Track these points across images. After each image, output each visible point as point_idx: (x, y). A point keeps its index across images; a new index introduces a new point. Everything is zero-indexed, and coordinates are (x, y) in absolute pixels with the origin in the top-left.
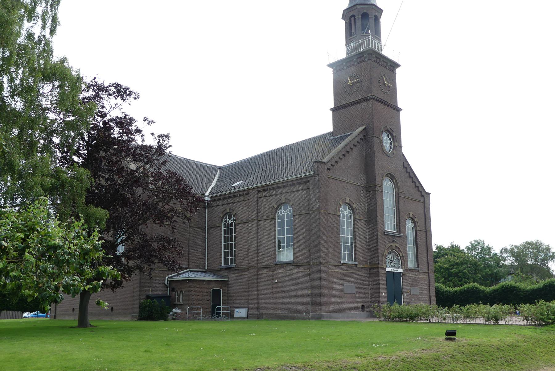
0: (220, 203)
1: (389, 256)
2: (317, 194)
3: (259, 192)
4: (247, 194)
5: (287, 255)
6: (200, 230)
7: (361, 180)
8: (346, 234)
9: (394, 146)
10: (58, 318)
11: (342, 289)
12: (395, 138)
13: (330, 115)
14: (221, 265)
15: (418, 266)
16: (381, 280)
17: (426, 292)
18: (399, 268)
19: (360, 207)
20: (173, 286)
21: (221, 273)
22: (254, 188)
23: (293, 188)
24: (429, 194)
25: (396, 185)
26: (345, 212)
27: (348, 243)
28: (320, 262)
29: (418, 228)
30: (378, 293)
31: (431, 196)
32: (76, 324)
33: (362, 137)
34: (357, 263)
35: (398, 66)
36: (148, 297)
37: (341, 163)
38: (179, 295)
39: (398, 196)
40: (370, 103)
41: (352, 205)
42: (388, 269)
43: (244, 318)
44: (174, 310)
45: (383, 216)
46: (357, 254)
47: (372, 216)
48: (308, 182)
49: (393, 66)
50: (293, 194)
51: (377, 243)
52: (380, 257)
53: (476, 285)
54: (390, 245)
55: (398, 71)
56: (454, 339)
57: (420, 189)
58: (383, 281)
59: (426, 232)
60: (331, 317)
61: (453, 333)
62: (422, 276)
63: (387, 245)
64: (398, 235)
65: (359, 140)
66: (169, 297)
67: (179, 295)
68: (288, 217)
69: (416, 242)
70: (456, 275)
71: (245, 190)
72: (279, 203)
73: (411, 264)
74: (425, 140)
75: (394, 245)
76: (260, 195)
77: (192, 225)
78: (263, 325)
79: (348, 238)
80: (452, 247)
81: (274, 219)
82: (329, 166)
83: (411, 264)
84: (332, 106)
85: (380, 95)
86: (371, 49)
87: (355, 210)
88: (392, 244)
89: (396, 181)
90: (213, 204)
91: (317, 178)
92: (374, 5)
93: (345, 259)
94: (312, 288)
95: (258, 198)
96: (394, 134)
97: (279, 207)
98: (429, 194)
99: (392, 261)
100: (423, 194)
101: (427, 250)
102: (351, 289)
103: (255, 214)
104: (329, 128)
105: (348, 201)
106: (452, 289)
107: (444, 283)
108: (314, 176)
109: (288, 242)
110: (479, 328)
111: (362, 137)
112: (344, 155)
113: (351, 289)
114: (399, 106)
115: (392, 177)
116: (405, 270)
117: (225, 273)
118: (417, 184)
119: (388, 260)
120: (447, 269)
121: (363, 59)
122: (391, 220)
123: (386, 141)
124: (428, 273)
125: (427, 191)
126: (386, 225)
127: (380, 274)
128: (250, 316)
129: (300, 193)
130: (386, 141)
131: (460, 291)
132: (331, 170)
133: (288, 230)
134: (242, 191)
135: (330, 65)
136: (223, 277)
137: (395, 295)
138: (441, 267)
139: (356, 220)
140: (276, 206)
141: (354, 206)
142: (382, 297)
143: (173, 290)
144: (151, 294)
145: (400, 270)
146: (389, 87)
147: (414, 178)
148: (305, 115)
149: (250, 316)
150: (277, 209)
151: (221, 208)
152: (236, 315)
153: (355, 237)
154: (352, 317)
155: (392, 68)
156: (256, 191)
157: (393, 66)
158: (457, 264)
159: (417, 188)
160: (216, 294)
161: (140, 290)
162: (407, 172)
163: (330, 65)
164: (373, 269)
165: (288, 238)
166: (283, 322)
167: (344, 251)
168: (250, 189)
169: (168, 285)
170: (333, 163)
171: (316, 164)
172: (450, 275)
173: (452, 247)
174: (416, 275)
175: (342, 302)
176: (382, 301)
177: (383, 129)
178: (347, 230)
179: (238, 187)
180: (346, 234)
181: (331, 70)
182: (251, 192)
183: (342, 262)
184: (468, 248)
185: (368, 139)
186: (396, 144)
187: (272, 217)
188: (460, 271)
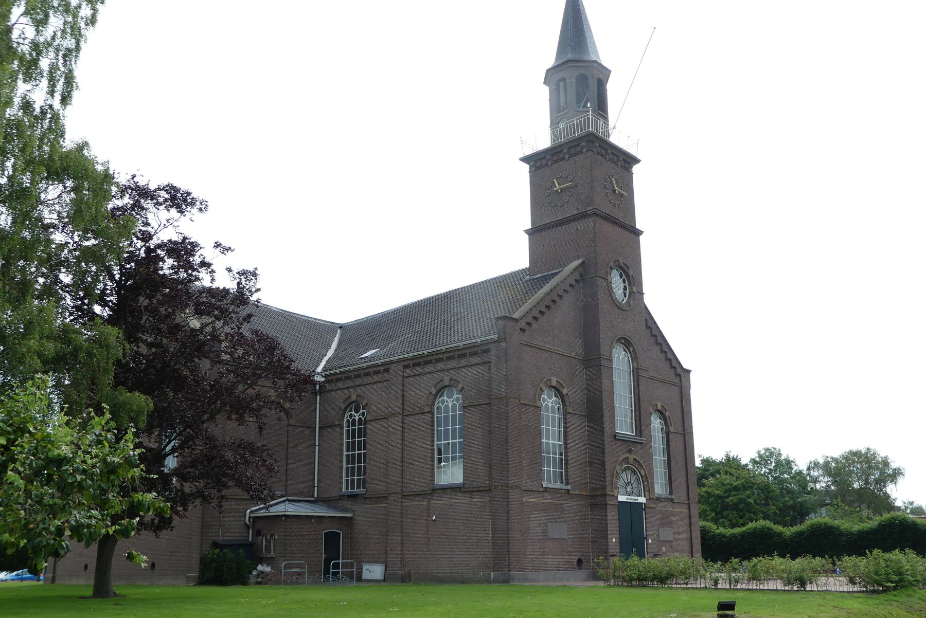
0: (340, 385)
1: (624, 475)
2: (503, 372)
4: (387, 370)
5: (452, 474)
6: (306, 431)
9: (631, 293)
10: (58, 582)
11: (545, 532)
14: (341, 490)
15: (671, 493)
16: (609, 516)
17: (685, 536)
18: (640, 495)
21: (340, 503)
22: (399, 361)
24: (688, 372)
25: (634, 357)
28: (507, 486)
29: (672, 429)
30: (605, 537)
32: (89, 592)
33: (578, 277)
34: (569, 487)
35: (636, 161)
36: (215, 545)
37: (542, 320)
41: (664, 411)
42: (622, 498)
44: (260, 567)
45: (612, 408)
50: (463, 371)
51: (603, 453)
55: (636, 169)
58: (612, 516)
60: (526, 580)
61: (731, 606)
62: (678, 509)
65: (573, 283)
66: (252, 545)
68: (454, 410)
69: (668, 451)
70: (735, 507)
71: (383, 364)
72: (440, 386)
73: (660, 489)
75: (631, 457)
76: (408, 372)
77: (292, 422)
81: (432, 412)
82: (523, 324)
83: (660, 489)
84: (529, 226)
85: (606, 209)
86: (592, 134)
87: (566, 398)
89: (634, 350)
91: (503, 344)
93: (549, 481)
95: (404, 377)
96: (631, 273)
97: (440, 392)
98: (688, 372)
99: (628, 483)
100: (679, 371)
102: (561, 531)
103: (399, 404)
105: (554, 384)
106: (729, 532)
107: (715, 521)
109: (454, 452)
110: (773, 596)
111: (578, 277)
112: (548, 307)
114: (639, 225)
115: (627, 344)
116: (650, 499)
117: (348, 504)
119: (621, 483)
120: (720, 497)
121: (578, 149)
122: (626, 416)
123: (617, 284)
124: (689, 504)
125: (685, 367)
126: (618, 424)
127: (608, 507)
128: (388, 578)
130: (617, 284)
131: (742, 535)
132: (527, 332)
133: (454, 430)
134: (377, 365)
135: (525, 159)
137: (633, 542)
138: (709, 494)
140: (434, 391)
141: (565, 391)
142: (612, 545)
143: (258, 533)
144: (220, 539)
145: (642, 500)
146: (622, 195)
148: (476, 235)
149: (388, 578)
152: (366, 575)
153: (566, 443)
154: (562, 579)
157: (628, 161)
158: (736, 488)
160: (332, 540)
162: (653, 336)
163: (525, 159)
164: (597, 498)
168: (392, 362)
169: (251, 525)
170: (530, 319)
172: (725, 507)
175: (544, 554)
176: (611, 552)
177: (611, 264)
179: (370, 359)
181: (526, 167)
182: (393, 367)
183: (545, 485)
184: (753, 461)
185: (588, 278)
186: (634, 289)
187: (427, 409)
188: (741, 501)
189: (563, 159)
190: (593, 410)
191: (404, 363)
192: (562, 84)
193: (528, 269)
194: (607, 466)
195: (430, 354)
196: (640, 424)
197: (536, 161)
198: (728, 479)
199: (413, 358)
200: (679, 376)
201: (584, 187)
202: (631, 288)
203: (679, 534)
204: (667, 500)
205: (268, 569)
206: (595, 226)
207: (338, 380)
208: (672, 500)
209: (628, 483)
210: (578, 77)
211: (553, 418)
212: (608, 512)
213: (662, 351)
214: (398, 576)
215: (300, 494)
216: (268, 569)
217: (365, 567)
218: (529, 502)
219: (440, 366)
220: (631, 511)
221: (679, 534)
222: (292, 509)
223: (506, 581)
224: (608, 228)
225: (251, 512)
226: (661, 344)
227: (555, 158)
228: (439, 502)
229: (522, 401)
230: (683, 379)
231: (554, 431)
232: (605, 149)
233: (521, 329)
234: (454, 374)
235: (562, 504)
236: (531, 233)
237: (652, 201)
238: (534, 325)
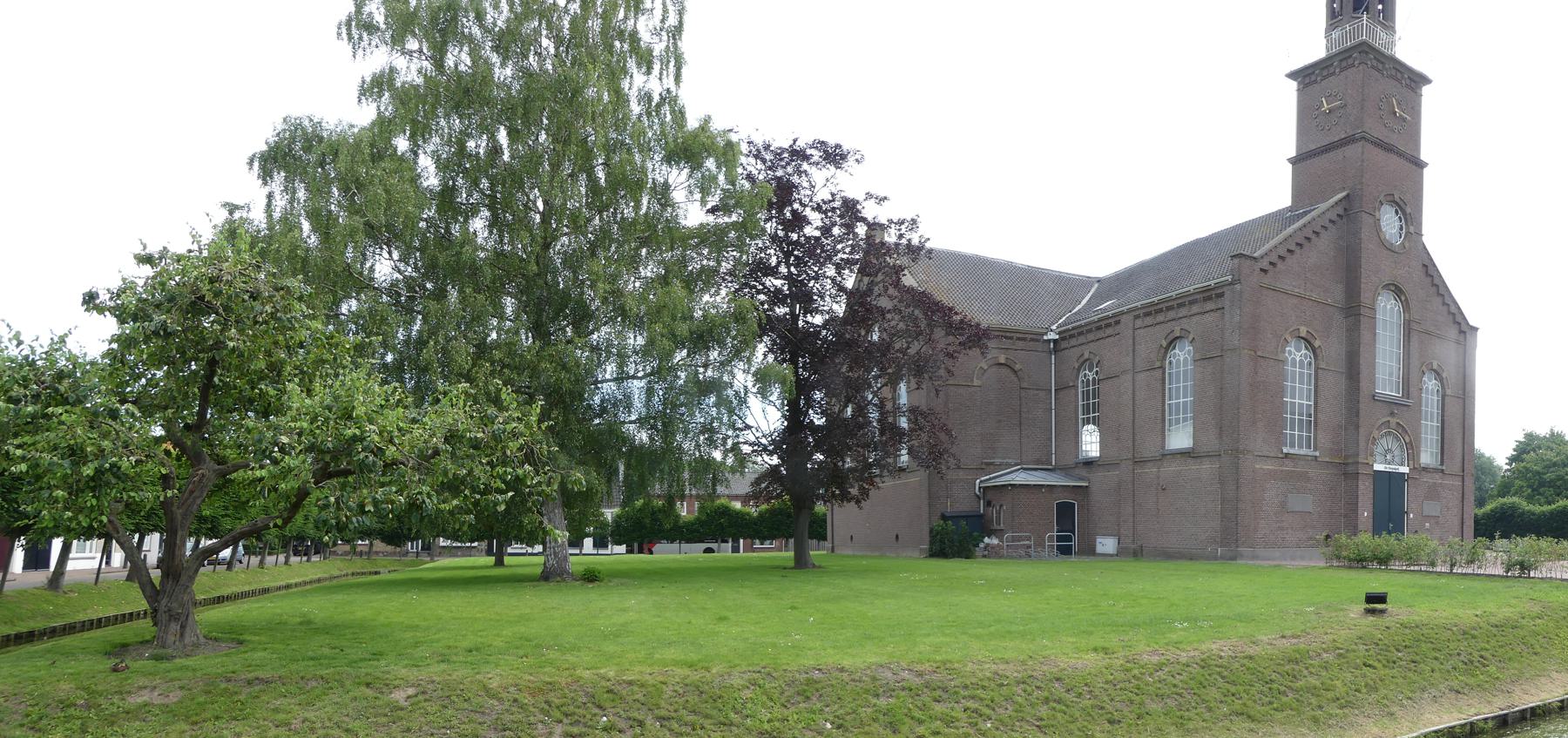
0: (1073, 342)
1: (1383, 441)
2: (1237, 318)
3: (1137, 317)
4: (1118, 323)
5: (1180, 439)
6: (1042, 394)
7: (1337, 294)
8: (1298, 396)
9: (1408, 233)
10: (837, 551)
11: (1283, 504)
12: (1410, 214)
16: (1361, 487)
17: (1456, 511)
19: (1334, 349)
20: (989, 497)
21: (1077, 471)
22: (1130, 311)
23: (1195, 309)
24: (1476, 329)
25: (1406, 307)
26: (1296, 354)
27: (1301, 414)
28: (1237, 450)
29: (1449, 392)
30: (1356, 511)
32: (792, 564)
33: (1341, 212)
35: (1425, 80)
36: (944, 517)
37: (1291, 260)
38: (999, 513)
39: (1408, 329)
42: (1378, 467)
44: (986, 540)
45: (1373, 365)
47: (1354, 369)
48: (1221, 295)
49: (1414, 81)
50: (1195, 319)
52: (1362, 444)
55: (1426, 90)
56: (1382, 611)
57: (1459, 319)
58: (1365, 489)
60: (1254, 557)
61: (1381, 599)
64: (1405, 401)
65: (1334, 218)
66: (981, 516)
67: (999, 513)
68: (1185, 364)
70: (1551, 484)
71: (1114, 316)
72: (1171, 337)
73: (1427, 458)
74: (1465, 220)
75: (1393, 421)
76: (1139, 323)
77: (1025, 385)
78: (1132, 566)
79: (1301, 405)
80: (1552, 434)
81: (1162, 368)
82: (1264, 264)
83: (1427, 458)
84: (1293, 154)
85: (1377, 132)
86: (1364, 43)
90: (1064, 345)
91: (1238, 287)
93: (1292, 446)
94: (1223, 500)
96: (1408, 210)
97: (1172, 343)
98: (1476, 329)
99: (1388, 451)
100: (1464, 328)
102: (1304, 502)
103: (1130, 359)
104: (1281, 198)
105: (1303, 334)
106: (1537, 509)
107: (1530, 499)
108: (1231, 284)
109: (1185, 412)
110: (1490, 585)
111: (1341, 212)
112: (1300, 245)
113: (1304, 502)
114: (1423, 157)
115: (1398, 291)
117: (1083, 472)
118: (1453, 309)
119: (1379, 449)
120: (1538, 473)
121: (1350, 61)
122: (1391, 375)
123: (1389, 222)
126: (1379, 383)
128: (1121, 553)
129: (1209, 318)
130: (1389, 222)
131: (1551, 513)
132: (1270, 274)
133: (1185, 387)
134: (1108, 318)
135: (1293, 75)
136: (1081, 479)
137: (1390, 516)
138: (1527, 469)
140: (1165, 344)
141: (1317, 344)
142: (1369, 516)
143: (988, 504)
144: (949, 511)
145: (1405, 470)
146: (1404, 120)
148: (1239, 171)
149: (1121, 553)
150: (1167, 349)
151: (1076, 352)
152: (1099, 549)
153: (1316, 404)
154: (1302, 558)
156: (1130, 317)
157: (1414, 81)
158: (1555, 464)
161: (930, 505)
162: (1434, 285)
163: (1293, 75)
164: (1347, 468)
165: (1185, 403)
166: (1171, 565)
167: (1293, 429)
168: (1122, 313)
170: (1274, 258)
171: (1236, 261)
172: (1542, 484)
173: (1552, 434)
175: (1281, 529)
176: (1361, 527)
178: (1301, 389)
179: (1105, 310)
180: (1298, 396)
181: (1294, 85)
182: (1124, 319)
183: (1285, 450)
185: (1351, 213)
186: (1412, 229)
187: (1158, 364)
188: (1560, 478)
193: (1290, 209)
195: (1160, 302)
196: (1408, 384)
197: (1306, 77)
198: (1551, 455)
199: (1143, 307)
200: (1464, 331)
201: (1359, 111)
204: (1435, 470)
205: (995, 541)
207: (1072, 336)
209: (1388, 451)
211: (1301, 374)
213: (1444, 304)
214: (1133, 551)
215: (1038, 462)
216: (995, 541)
217: (1099, 540)
218: (626, 476)
219: (1171, 314)
220: (1389, 485)
222: (1020, 478)
223: (1233, 558)
224: (1378, 155)
228: (1170, 468)
231: (1301, 389)
234: (1185, 324)
236: (1294, 162)
237: (1442, 131)
238: (1280, 265)
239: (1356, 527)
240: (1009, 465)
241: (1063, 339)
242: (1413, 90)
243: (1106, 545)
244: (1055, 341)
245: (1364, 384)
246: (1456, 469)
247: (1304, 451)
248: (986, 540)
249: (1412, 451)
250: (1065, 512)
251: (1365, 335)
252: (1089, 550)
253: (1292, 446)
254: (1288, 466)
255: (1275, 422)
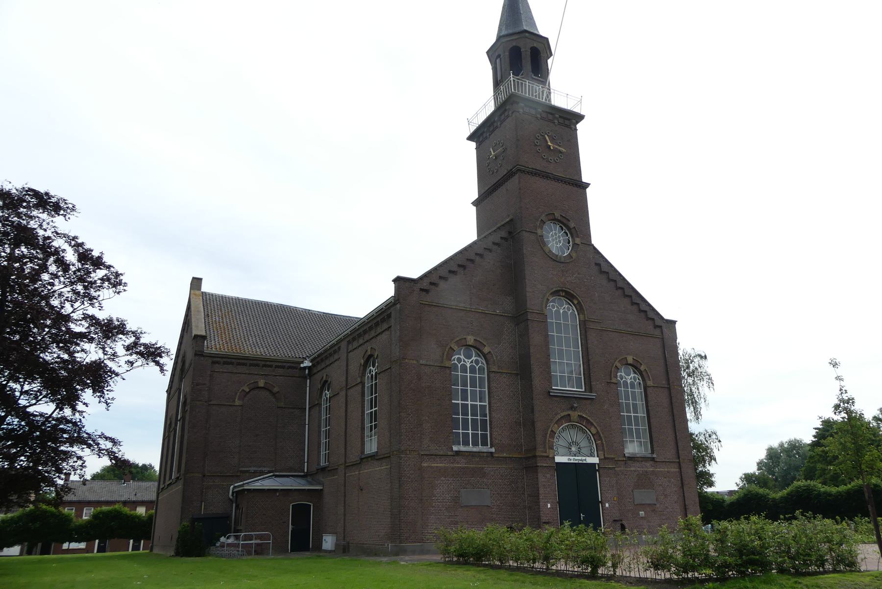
3: (349, 343)
13: (471, 214)
14: (319, 464)
15: (653, 452)
18: (592, 455)
24: (673, 323)
25: (580, 310)
30: (537, 502)
31: (677, 326)
34: (493, 450)
35: (579, 117)
40: (515, 180)
41: (638, 366)
42: (559, 459)
43: (330, 552)
44: (222, 539)
46: (495, 434)
51: (533, 412)
52: (539, 438)
53: (802, 483)
54: (565, 413)
57: (651, 315)
59: (669, 389)
62: (663, 469)
63: (556, 414)
64: (588, 395)
69: (647, 406)
75: (574, 415)
84: (475, 196)
87: (488, 357)
88: (570, 412)
89: (579, 303)
91: (398, 306)
92: (526, 31)
95: (348, 353)
98: (673, 323)
101: (674, 421)
106: (834, 490)
116: (605, 458)
118: (643, 307)
121: (506, 114)
123: (556, 241)
124: (679, 462)
125: (666, 317)
127: (539, 470)
129: (385, 336)
130: (556, 241)
131: (848, 492)
135: (470, 138)
139: (492, 375)
140: (362, 362)
145: (595, 460)
147: (634, 297)
148: (436, 217)
155: (567, 122)
159: (643, 314)
160: (301, 513)
162: (618, 288)
163: (470, 138)
164: (528, 459)
169: (234, 500)
174: (649, 467)
177: (543, 217)
181: (473, 145)
183: (455, 448)
184: (876, 418)
187: (359, 380)
189: (497, 127)
190: (523, 368)
191: (347, 339)
192: (498, 61)
194: (538, 425)
201: (529, 157)
202: (574, 240)
203: (666, 496)
204: (644, 459)
206: (519, 183)
208: (653, 459)
210: (521, 53)
212: (540, 475)
214: (344, 549)
218: (432, 467)
221: (666, 496)
224: (539, 183)
225: (235, 487)
226: (630, 296)
227: (491, 129)
229: (421, 362)
230: (665, 330)
232: (569, 120)
233: (422, 290)
235: (483, 468)
236: (476, 203)
237: (597, 156)
239: (539, 518)
240: (262, 473)
241: (313, 365)
242: (568, 126)
243: (328, 542)
244: (309, 368)
245: (537, 382)
246: (670, 454)
247: (480, 448)
248: (222, 539)
249: (607, 441)
250: (301, 513)
251: (535, 338)
252: (318, 547)
253: (466, 443)
254: (462, 463)
255: (447, 420)
